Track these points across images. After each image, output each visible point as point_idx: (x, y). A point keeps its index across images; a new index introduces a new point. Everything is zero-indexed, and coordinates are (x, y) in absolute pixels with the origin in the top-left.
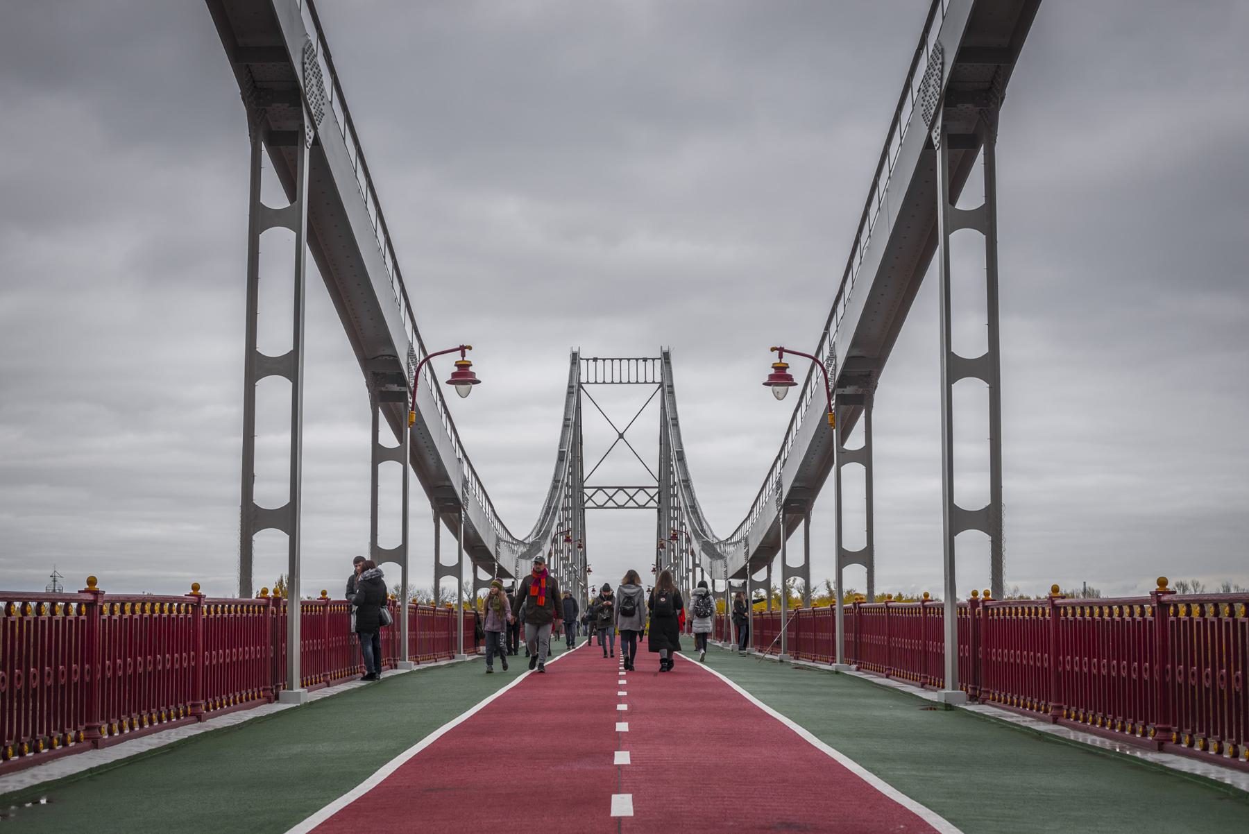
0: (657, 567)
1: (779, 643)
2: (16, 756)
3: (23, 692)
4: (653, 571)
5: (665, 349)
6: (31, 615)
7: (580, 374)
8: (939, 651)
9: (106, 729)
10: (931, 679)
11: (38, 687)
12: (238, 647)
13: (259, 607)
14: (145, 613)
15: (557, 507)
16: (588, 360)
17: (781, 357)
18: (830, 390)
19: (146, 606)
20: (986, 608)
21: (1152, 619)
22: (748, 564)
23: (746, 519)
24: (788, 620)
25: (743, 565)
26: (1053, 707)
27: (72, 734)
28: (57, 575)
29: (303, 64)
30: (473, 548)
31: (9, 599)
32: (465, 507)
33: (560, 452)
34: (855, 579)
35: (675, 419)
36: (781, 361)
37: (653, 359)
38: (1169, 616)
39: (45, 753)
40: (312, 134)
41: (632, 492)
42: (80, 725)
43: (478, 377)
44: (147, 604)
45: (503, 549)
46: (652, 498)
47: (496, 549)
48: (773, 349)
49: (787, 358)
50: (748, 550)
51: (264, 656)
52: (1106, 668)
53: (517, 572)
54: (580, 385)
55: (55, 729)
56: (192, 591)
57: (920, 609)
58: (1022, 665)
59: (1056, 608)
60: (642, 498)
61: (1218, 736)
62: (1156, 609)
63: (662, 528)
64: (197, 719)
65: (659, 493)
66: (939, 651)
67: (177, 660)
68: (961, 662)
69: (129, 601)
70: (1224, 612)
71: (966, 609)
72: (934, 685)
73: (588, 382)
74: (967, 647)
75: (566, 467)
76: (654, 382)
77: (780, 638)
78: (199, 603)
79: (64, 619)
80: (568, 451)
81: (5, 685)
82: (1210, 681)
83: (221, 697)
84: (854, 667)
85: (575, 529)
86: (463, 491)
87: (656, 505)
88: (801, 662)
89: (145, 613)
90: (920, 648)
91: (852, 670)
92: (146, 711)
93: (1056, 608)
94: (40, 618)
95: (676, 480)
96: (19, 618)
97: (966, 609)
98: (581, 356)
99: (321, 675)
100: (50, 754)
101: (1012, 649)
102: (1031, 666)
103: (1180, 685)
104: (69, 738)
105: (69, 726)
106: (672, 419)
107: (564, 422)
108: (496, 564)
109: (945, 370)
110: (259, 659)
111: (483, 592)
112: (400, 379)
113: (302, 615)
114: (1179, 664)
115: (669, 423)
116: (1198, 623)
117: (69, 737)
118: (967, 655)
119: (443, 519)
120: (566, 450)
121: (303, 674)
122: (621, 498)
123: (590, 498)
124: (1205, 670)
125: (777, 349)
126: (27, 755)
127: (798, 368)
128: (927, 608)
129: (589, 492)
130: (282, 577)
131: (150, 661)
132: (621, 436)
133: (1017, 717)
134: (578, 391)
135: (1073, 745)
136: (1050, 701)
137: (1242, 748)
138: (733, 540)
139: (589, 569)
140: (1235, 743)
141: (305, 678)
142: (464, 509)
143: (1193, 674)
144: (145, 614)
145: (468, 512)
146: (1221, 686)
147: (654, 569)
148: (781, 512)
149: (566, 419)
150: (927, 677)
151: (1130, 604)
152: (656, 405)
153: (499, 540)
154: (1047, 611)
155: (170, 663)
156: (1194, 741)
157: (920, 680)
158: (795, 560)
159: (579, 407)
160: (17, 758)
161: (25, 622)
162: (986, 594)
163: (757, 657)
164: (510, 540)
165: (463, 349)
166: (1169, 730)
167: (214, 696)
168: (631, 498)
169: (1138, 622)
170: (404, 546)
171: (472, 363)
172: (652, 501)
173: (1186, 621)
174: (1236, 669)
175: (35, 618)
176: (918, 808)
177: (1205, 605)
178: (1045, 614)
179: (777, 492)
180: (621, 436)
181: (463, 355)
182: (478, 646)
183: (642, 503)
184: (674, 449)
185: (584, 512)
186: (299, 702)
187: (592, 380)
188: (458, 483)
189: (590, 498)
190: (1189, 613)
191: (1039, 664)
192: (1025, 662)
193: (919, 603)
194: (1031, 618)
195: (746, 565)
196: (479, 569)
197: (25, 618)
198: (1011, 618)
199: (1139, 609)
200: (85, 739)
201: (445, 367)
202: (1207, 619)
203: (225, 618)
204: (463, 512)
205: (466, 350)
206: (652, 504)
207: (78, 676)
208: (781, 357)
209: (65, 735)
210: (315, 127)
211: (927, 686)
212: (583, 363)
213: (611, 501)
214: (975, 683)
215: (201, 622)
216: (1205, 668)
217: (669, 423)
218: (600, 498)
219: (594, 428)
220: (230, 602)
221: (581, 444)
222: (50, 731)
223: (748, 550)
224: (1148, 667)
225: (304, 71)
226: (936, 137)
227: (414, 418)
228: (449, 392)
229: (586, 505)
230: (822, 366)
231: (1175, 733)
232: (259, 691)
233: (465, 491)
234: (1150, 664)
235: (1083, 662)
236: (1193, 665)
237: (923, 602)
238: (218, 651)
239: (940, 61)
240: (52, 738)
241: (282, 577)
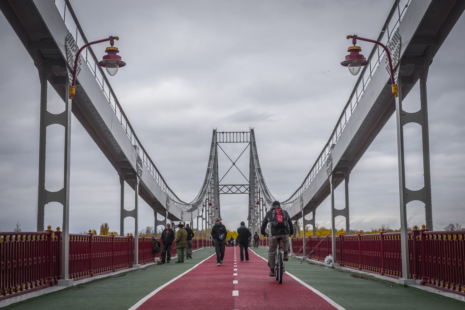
0: (249, 218)
1: (302, 252)
2: (14, 292)
3: (5, 270)
4: (247, 219)
5: (252, 128)
6: (14, 240)
7: (217, 139)
8: (398, 257)
9: (34, 285)
10: (364, 266)
11: (22, 266)
12: (97, 253)
13: (110, 238)
14: (71, 240)
15: (206, 191)
16: (220, 133)
17: (354, 43)
18: (393, 68)
19: (42, 236)
20: (424, 235)
21: (413, 239)
22: (303, 211)
23: (300, 188)
24: (306, 241)
25: (299, 212)
26: (382, 270)
27: (19, 287)
28: (19, 225)
30: (154, 203)
31: (5, 235)
32: (139, 175)
33: (208, 169)
34: (340, 223)
35: (257, 156)
36: (355, 45)
37: (247, 132)
38: (384, 239)
39: (24, 291)
42: (17, 284)
44: (34, 236)
45: (171, 204)
46: (247, 189)
47: (167, 204)
48: (348, 37)
49: (359, 43)
50: (303, 203)
51: (89, 257)
52: (412, 257)
53: (182, 218)
54: (217, 143)
55: (12, 285)
56: (48, 229)
57: (358, 238)
58: (388, 258)
59: (383, 236)
60: (243, 189)
61: (454, 283)
62: (414, 236)
63: (251, 203)
64: (129, 267)
65: (250, 187)
66: (398, 257)
67: (73, 257)
68: (411, 262)
69: (34, 234)
70: (444, 238)
71: (379, 237)
72: (352, 266)
73: (220, 142)
74: (358, 251)
75: (211, 175)
76: (247, 142)
77: (303, 249)
78: (91, 236)
79: (9, 242)
80: (211, 168)
81: (10, 266)
82: (450, 262)
83: (73, 274)
84: (419, 281)
85: (215, 202)
86: (137, 165)
87: (248, 192)
88: (343, 268)
89: (71, 240)
90: (339, 252)
91: (417, 284)
92: (72, 274)
93: (383, 236)
94: (11, 242)
96: (20, 241)
97: (379, 237)
98: (217, 131)
99: (88, 271)
100: (16, 294)
101: (389, 252)
102: (395, 259)
103: (398, 259)
104: (18, 289)
105: (18, 284)
106: (255, 155)
107: (210, 157)
108: (167, 212)
110: (103, 258)
111: (161, 228)
112: (62, 63)
113: (70, 242)
114: (439, 256)
115: (254, 157)
116: (445, 242)
117: (17, 288)
118: (380, 256)
119: (125, 181)
120: (210, 168)
121: (70, 272)
122: (234, 189)
123: (221, 190)
124: (448, 259)
126: (18, 292)
128: (361, 237)
129: (221, 187)
130: (103, 224)
131: (44, 258)
133: (428, 290)
134: (216, 146)
135: (441, 297)
136: (382, 268)
137: (463, 288)
138: (290, 201)
139: (221, 219)
140: (460, 286)
141: (72, 274)
142: (138, 176)
144: (71, 241)
145: (143, 178)
146: (460, 265)
147: (248, 218)
148: (331, 176)
149: (211, 156)
150: (344, 262)
151: (442, 234)
152: (247, 153)
153: (168, 201)
154: (380, 237)
155: (71, 258)
156: (445, 285)
157: (339, 263)
158: (340, 205)
159: (216, 152)
160: (14, 293)
161: (5, 243)
162: (423, 227)
163: (308, 262)
164: (178, 201)
165: (112, 39)
166: (427, 279)
167: (85, 271)
168: (238, 189)
169: (431, 241)
170: (136, 210)
171: (119, 50)
172: (247, 190)
173: (451, 242)
174: (454, 258)
175: (3, 242)
176: (328, 300)
177: (453, 235)
178: (392, 238)
179: (327, 165)
181: (112, 44)
182: (154, 257)
183: (243, 191)
184: (256, 167)
185: (219, 196)
186: (139, 267)
187: (222, 141)
188: (132, 158)
189: (221, 190)
190: (442, 238)
191: (395, 257)
192: (369, 255)
193: (412, 232)
194: (372, 240)
195: (301, 212)
196: (158, 214)
197: (17, 241)
198: (377, 240)
199: (436, 236)
200: (47, 282)
202: (454, 240)
203: (75, 242)
204: (137, 178)
205: (115, 40)
206: (247, 192)
207: (16, 265)
208: (354, 43)
209: (16, 288)
211: (362, 269)
212: (218, 134)
213: (230, 191)
214: (384, 268)
215: (92, 243)
216: (443, 258)
217: (254, 157)
218: (225, 189)
219: (223, 165)
220: (32, 234)
221: (218, 168)
222: (16, 285)
223: (303, 203)
224: (440, 259)
227: (74, 92)
229: (220, 192)
230: (385, 48)
231: (429, 280)
232: (88, 272)
233: (139, 165)
234: (441, 257)
235: (410, 256)
236: (444, 257)
237: (381, 233)
238: (97, 253)
240: (10, 289)
241: (103, 224)
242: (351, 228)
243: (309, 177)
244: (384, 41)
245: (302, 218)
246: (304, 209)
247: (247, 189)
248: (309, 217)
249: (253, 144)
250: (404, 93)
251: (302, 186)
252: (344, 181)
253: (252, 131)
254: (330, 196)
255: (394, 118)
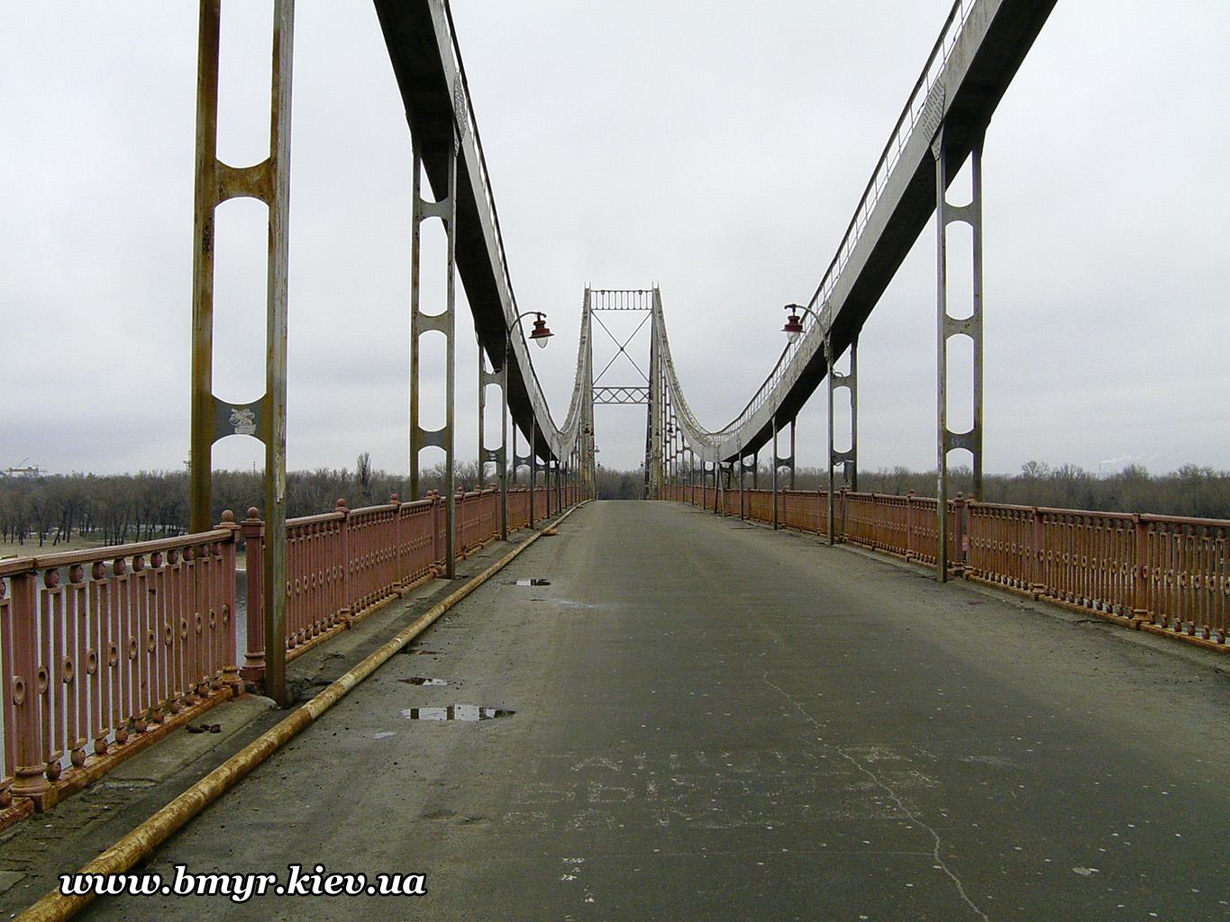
17: (794, 311)
29: (455, 92)
40: (458, 145)
41: (630, 391)
43: (551, 332)
46: (645, 396)
54: (591, 311)
60: (638, 396)
95: (668, 384)
109: (450, 171)
115: (659, 338)
122: (622, 396)
125: (790, 306)
127: (808, 324)
132: (622, 349)
143: (1103, 563)
149: (583, 337)
180: (622, 349)
201: (528, 325)
206: (646, 400)
210: (460, 140)
212: (593, 294)
217: (659, 338)
218: (606, 396)
225: (455, 97)
226: (936, 151)
228: (532, 343)
239: (943, 93)
242: (985, 471)
243: (763, 391)
244: (814, 309)
245: (739, 461)
246: (742, 451)
247: (645, 396)
248: (748, 461)
249: (657, 312)
250: (836, 355)
251: (740, 418)
252: (790, 423)
253: (656, 293)
254: (772, 439)
255: (825, 381)
